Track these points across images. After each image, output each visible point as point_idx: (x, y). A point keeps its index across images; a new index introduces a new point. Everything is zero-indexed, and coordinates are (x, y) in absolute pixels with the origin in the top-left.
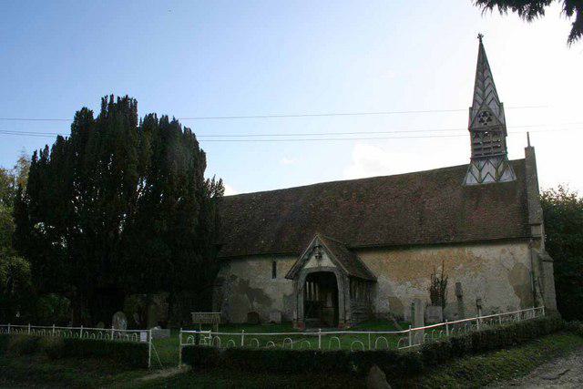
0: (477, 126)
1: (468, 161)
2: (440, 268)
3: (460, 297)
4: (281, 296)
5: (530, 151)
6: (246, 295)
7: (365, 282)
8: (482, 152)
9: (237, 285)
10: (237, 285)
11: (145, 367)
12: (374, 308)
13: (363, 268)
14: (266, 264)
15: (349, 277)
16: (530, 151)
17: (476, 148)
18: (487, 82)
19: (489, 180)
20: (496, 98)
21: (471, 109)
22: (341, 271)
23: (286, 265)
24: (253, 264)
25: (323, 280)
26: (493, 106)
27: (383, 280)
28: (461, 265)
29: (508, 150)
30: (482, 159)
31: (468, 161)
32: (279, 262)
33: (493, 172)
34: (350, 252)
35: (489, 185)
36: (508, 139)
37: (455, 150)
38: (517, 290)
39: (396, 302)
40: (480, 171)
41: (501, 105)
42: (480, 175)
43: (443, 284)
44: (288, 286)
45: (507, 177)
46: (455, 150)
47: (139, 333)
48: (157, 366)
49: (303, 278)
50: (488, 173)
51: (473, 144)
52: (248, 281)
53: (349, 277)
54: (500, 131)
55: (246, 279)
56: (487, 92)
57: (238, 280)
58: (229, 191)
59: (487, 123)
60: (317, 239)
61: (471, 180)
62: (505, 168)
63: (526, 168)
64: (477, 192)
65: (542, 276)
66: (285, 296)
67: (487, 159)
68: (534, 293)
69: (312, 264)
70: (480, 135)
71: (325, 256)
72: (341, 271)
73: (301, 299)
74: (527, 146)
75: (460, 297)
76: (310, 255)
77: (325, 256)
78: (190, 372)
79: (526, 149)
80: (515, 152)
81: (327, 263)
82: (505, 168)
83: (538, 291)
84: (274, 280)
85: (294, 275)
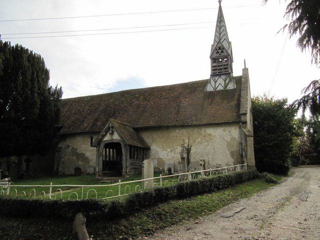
2: (187, 140)
5: (245, 70)
6: (75, 157)
8: (217, 71)
16: (245, 70)
19: (220, 88)
20: (227, 39)
22: (124, 141)
24: (79, 139)
26: (225, 44)
30: (216, 75)
33: (223, 83)
37: (199, 70)
38: (232, 154)
40: (215, 82)
41: (229, 43)
45: (231, 86)
46: (199, 70)
49: (102, 146)
50: (220, 84)
51: (213, 67)
54: (229, 58)
56: (222, 35)
57: (71, 148)
58: (64, 97)
59: (221, 57)
61: (209, 88)
62: (230, 81)
67: (220, 75)
69: (107, 138)
70: (217, 61)
71: (115, 133)
74: (243, 68)
79: (243, 70)
80: (237, 72)
81: (116, 137)
82: (230, 81)
83: (244, 154)
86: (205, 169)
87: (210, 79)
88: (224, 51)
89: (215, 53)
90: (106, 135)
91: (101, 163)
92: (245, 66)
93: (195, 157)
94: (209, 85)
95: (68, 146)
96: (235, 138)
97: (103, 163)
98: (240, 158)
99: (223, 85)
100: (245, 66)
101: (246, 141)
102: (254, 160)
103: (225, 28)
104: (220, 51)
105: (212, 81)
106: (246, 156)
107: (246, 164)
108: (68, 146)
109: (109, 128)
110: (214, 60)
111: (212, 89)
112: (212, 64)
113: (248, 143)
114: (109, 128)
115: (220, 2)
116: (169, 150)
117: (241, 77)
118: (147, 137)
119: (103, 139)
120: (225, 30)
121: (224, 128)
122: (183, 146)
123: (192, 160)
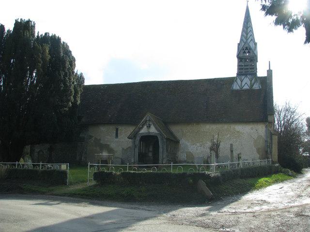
0: (241, 55)
1: (235, 75)
2: (216, 136)
3: (232, 151)
4: (121, 149)
5: (270, 72)
6: (98, 148)
7: (174, 142)
8: (244, 71)
9: (92, 141)
10: (92, 141)
11: (65, 184)
12: (177, 157)
13: (171, 133)
14: (111, 129)
15: (167, 139)
16: (270, 72)
17: (240, 67)
18: (249, 30)
19: (246, 87)
20: (253, 40)
21: (239, 44)
22: (161, 135)
23: (126, 131)
24: (103, 129)
25: (149, 140)
26: (252, 45)
27: (183, 142)
28: (229, 135)
29: (257, 70)
30: (243, 75)
31: (235, 75)
32: (120, 128)
33: (249, 83)
34: (166, 123)
35: (246, 90)
36: (258, 64)
37: (228, 69)
38: (258, 150)
39: (190, 156)
40: (242, 82)
41: (256, 44)
42: (241, 84)
43: (218, 146)
44: (129, 143)
45: (256, 86)
46: (228, 69)
47: (230, 127)
48: (71, 184)
49: (138, 138)
50: (246, 83)
51: (239, 66)
52: (100, 139)
53: (167, 139)
54: (254, 59)
55: (99, 138)
56: (249, 35)
57: (93, 139)
58: (87, 82)
59: (247, 55)
60: (148, 116)
61: (236, 87)
62: (256, 81)
63: (266, 83)
64: (239, 93)
65: (271, 143)
66: (123, 149)
67: (246, 75)
68: (267, 152)
69: (144, 131)
70: (243, 60)
71: (152, 126)
72: (161, 135)
73: (137, 150)
74: (268, 69)
75: (232, 151)
76: (143, 126)
77: (152, 126)
78: (95, 186)
79: (268, 71)
80: (261, 72)
81: (153, 130)
82: (256, 81)
83: (269, 151)
84: (117, 140)
85: (133, 136)
86: (232, 161)
87: (236, 77)
88: (251, 51)
89: (242, 53)
90: (142, 128)
91: (137, 154)
92: (270, 68)
93: (224, 147)
94: (235, 83)
95: (91, 137)
96: (262, 136)
97: (139, 155)
98: (265, 153)
99: (249, 86)
100: (270, 68)
101: (271, 139)
102: (277, 156)
103: (253, 33)
104: (247, 51)
105: (238, 79)
106: (271, 153)
107: (271, 160)
108: (91, 137)
109: (146, 121)
110: (240, 58)
111: (238, 88)
112: (238, 64)
113: (273, 141)
114: (146, 121)
115: (248, 1)
116: (198, 144)
117: (265, 78)
118: (176, 130)
119: (139, 131)
120: (252, 31)
121: (251, 127)
122: (212, 141)
123: (220, 155)
